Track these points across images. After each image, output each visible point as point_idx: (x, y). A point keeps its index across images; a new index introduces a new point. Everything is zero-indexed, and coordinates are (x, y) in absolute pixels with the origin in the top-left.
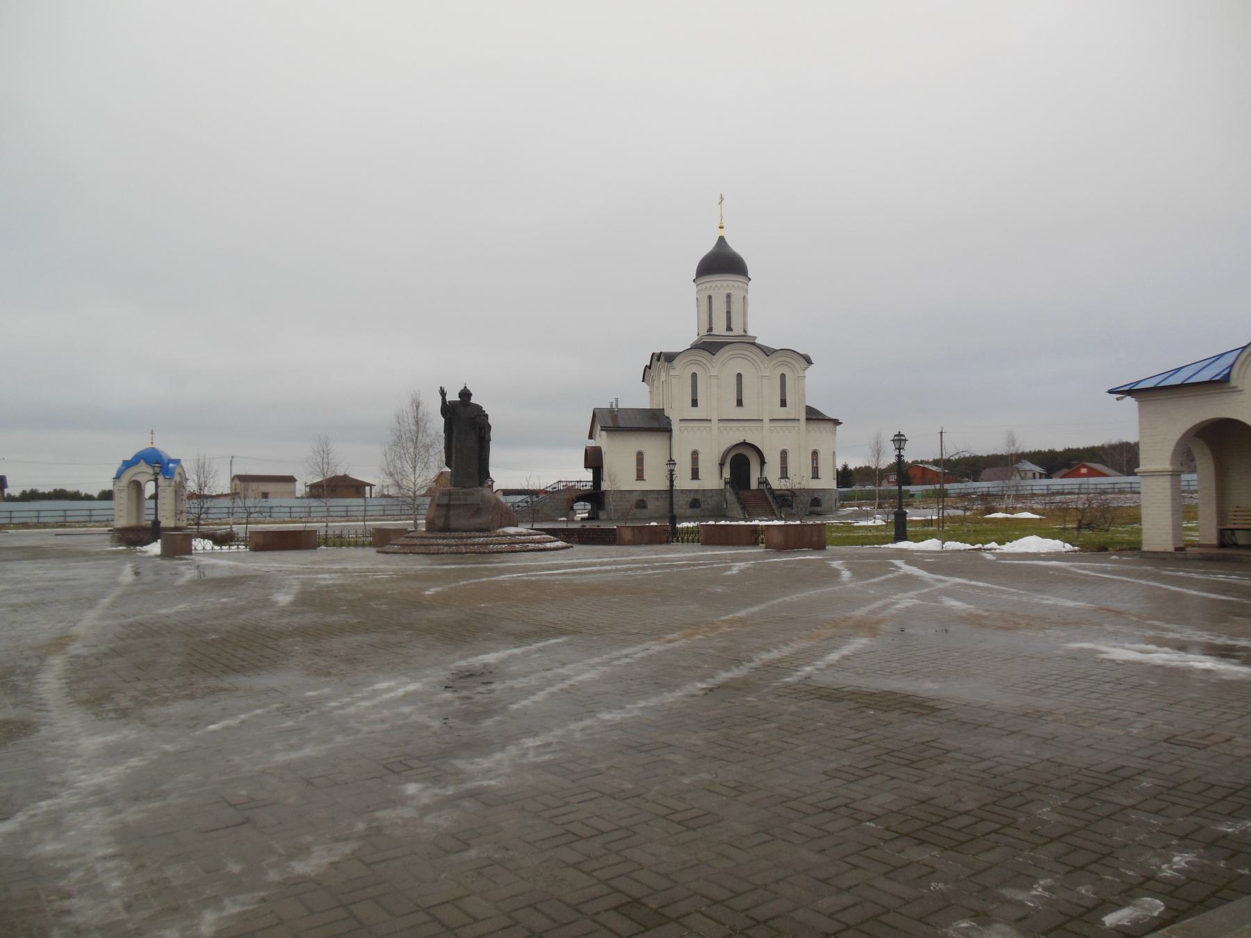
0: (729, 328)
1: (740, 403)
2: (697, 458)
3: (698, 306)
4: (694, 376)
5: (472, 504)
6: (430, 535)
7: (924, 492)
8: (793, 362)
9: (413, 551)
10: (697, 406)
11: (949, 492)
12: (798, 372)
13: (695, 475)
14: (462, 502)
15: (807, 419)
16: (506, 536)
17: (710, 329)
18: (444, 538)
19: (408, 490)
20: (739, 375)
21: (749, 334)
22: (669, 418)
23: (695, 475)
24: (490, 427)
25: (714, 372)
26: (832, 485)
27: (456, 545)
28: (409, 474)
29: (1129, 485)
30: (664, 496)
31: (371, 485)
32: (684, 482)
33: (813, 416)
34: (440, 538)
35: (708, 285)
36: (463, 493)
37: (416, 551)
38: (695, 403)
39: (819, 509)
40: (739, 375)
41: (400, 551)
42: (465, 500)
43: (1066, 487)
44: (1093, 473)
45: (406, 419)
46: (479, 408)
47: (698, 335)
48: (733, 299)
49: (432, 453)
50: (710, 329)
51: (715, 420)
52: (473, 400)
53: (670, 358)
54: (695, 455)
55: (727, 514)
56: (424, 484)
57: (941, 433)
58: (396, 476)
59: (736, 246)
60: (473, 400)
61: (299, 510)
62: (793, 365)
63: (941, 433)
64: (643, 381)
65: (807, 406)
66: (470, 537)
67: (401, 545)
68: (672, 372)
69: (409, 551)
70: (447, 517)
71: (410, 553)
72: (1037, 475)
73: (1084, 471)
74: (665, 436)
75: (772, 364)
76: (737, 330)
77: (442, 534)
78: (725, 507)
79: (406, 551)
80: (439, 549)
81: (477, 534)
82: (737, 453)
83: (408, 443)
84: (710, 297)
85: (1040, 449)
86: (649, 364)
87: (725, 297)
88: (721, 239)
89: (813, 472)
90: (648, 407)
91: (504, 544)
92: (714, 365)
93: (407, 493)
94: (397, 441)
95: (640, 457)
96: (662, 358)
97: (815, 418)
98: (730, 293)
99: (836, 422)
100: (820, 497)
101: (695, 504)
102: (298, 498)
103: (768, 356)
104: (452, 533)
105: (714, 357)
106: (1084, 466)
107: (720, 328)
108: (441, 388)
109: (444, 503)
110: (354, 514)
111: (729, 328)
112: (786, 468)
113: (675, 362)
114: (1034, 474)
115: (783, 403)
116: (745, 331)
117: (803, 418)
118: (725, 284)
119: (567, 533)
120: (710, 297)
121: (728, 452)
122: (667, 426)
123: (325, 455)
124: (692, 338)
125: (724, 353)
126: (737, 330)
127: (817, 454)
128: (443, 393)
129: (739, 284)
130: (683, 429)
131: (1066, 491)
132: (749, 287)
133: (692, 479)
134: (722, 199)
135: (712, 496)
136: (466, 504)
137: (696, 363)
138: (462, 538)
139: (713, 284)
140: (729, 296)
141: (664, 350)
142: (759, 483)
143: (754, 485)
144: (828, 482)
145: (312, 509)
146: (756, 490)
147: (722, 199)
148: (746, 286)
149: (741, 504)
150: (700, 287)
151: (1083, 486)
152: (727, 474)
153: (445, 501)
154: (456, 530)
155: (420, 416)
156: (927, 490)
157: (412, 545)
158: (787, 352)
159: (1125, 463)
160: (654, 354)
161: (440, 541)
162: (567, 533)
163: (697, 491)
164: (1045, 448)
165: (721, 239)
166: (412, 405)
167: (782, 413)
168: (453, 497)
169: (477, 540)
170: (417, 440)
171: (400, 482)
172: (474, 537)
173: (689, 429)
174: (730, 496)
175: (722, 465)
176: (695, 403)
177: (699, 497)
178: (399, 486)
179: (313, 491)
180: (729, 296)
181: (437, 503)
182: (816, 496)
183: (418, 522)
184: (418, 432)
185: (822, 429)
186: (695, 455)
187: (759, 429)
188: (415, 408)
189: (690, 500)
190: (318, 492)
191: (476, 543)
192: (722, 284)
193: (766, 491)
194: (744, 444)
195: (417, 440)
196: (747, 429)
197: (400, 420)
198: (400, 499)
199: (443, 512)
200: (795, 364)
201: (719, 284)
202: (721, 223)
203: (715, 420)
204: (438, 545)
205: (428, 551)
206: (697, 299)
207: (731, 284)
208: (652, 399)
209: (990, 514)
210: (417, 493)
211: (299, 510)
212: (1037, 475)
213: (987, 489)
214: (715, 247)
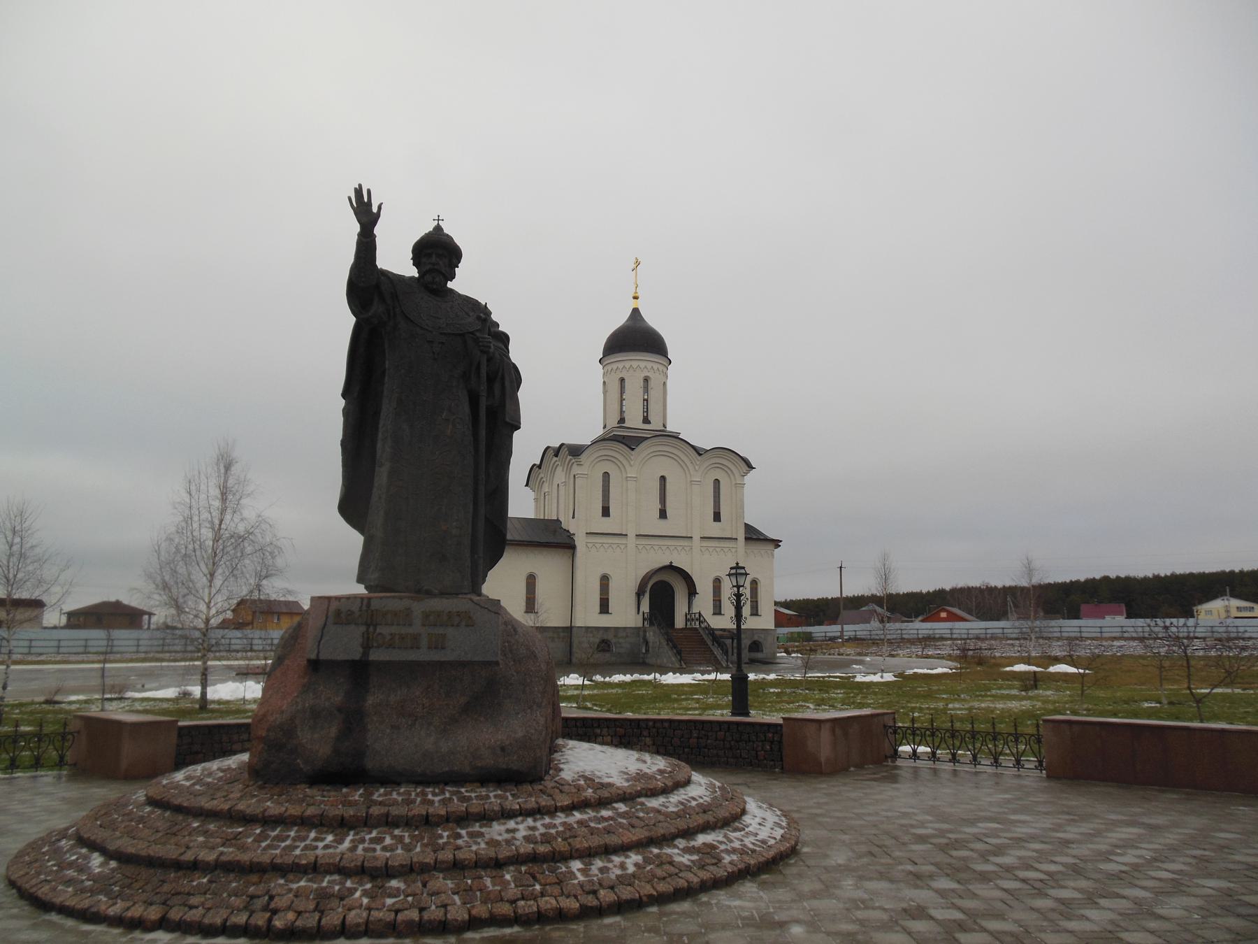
0: (646, 420)
1: (663, 514)
2: (608, 585)
3: (605, 392)
4: (606, 475)
5: (463, 664)
6: (272, 807)
7: (789, 636)
8: (730, 465)
9: (175, 914)
10: (609, 516)
11: (813, 635)
12: (735, 479)
13: (604, 607)
14: (423, 655)
15: (746, 539)
16: (602, 803)
17: (622, 420)
18: (342, 825)
19: (196, 616)
20: (663, 479)
21: (668, 429)
22: (568, 531)
23: (604, 607)
24: (514, 377)
25: (632, 473)
26: (770, 625)
27: (409, 871)
28: (199, 585)
29: (1000, 631)
30: (562, 634)
31: (150, 614)
32: (588, 616)
33: (753, 536)
34: (321, 823)
35: (620, 365)
36: (426, 615)
37: (193, 915)
38: (606, 512)
39: (759, 655)
40: (663, 479)
41: (102, 902)
42: (438, 644)
43: (937, 631)
44: (953, 618)
45: (203, 487)
46: (479, 312)
47: (605, 427)
48: (652, 384)
49: (249, 549)
50: (622, 420)
51: (632, 535)
52: (463, 282)
53: (576, 451)
54: (605, 580)
55: (647, 661)
56: (226, 605)
57: (841, 567)
58: (174, 590)
59: (653, 319)
60: (463, 282)
61: (71, 643)
62: (731, 471)
63: (841, 567)
64: (527, 485)
65: (746, 525)
66: (463, 819)
67: (124, 858)
68: (576, 470)
69: (154, 913)
70: (353, 720)
71: (163, 924)
72: (885, 619)
73: (943, 615)
74: (569, 552)
75: (707, 464)
76: (655, 424)
77: (325, 801)
78: (644, 651)
79: (137, 911)
80: (323, 897)
81: (494, 797)
82: (659, 579)
83: (203, 531)
84: (622, 380)
85: (1232, 568)
86: (538, 463)
87: (642, 381)
88: (636, 311)
89: (715, 606)
90: (531, 515)
91: (624, 849)
92: (632, 463)
93: (192, 622)
94: (183, 524)
95: (531, 581)
96: (564, 451)
97: (755, 537)
98: (648, 376)
99: (776, 543)
100: (760, 640)
101: (604, 646)
102: (46, 628)
103: (700, 455)
104: (379, 794)
105: (633, 453)
106: (944, 610)
107: (634, 420)
108: (359, 192)
109: (341, 656)
110: (121, 649)
111: (646, 420)
112: (757, 602)
113: (583, 457)
114: (883, 618)
115: (717, 517)
116: (665, 426)
117: (741, 535)
118: (642, 364)
119: (621, 731)
120: (622, 380)
121: (650, 578)
122: (567, 541)
123: (17, 540)
124: (599, 432)
125: (643, 450)
126: (655, 424)
127: (757, 584)
128: (366, 214)
129: (652, 364)
130: (590, 545)
131: (937, 636)
132: (669, 372)
133: (601, 613)
134: (638, 263)
135: (627, 636)
136: (441, 665)
137: (609, 459)
138: (428, 822)
139: (627, 364)
140: (646, 380)
141: (567, 442)
142: (687, 620)
143: (679, 622)
144: (765, 621)
145: (62, 643)
146: (682, 629)
147: (638, 263)
148: (665, 369)
149: (675, 646)
150: (609, 367)
151: (874, 632)
152: (645, 607)
153: (346, 645)
154: (390, 779)
155: (231, 482)
156: (792, 633)
157: (178, 865)
158: (721, 452)
159: (974, 608)
160: (548, 448)
161: (325, 846)
162: (621, 731)
163: (606, 629)
164: (800, 597)
165: (636, 311)
166: (217, 464)
167: (715, 529)
168: (384, 630)
169: (497, 830)
170: (220, 525)
171: (181, 600)
172: (486, 818)
173: (606, 546)
174: (653, 636)
175: (639, 594)
176: (606, 512)
177: (610, 637)
178: (179, 609)
179: (72, 619)
180: (646, 380)
181: (313, 657)
182: (756, 638)
183: (209, 663)
184: (223, 511)
185: (763, 552)
186: (605, 580)
187: (687, 549)
188: (223, 471)
189: (597, 641)
190: (79, 620)
191: (504, 853)
192: (637, 364)
193: (700, 630)
194: (671, 568)
195: (220, 525)
196: (672, 548)
197: (193, 488)
198: (177, 632)
199: (332, 694)
200: (730, 465)
201: (635, 364)
202: (636, 293)
203: (632, 535)
204: (315, 869)
205: (260, 920)
206: (604, 383)
207: (649, 365)
208: (537, 508)
209: (1035, 672)
210: (212, 621)
211: (71, 643)
212: (885, 619)
213: (854, 633)
214: (627, 321)
